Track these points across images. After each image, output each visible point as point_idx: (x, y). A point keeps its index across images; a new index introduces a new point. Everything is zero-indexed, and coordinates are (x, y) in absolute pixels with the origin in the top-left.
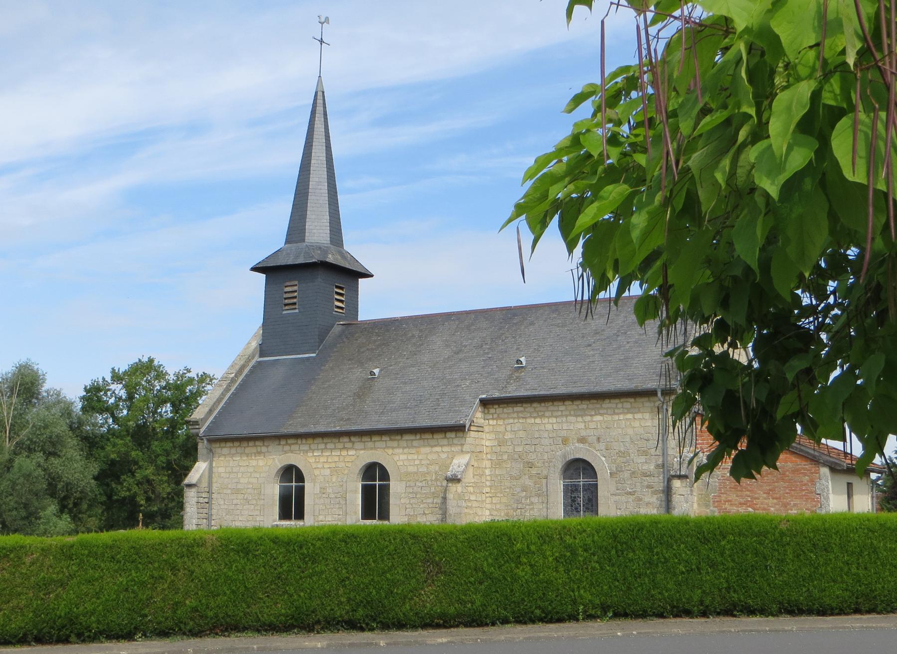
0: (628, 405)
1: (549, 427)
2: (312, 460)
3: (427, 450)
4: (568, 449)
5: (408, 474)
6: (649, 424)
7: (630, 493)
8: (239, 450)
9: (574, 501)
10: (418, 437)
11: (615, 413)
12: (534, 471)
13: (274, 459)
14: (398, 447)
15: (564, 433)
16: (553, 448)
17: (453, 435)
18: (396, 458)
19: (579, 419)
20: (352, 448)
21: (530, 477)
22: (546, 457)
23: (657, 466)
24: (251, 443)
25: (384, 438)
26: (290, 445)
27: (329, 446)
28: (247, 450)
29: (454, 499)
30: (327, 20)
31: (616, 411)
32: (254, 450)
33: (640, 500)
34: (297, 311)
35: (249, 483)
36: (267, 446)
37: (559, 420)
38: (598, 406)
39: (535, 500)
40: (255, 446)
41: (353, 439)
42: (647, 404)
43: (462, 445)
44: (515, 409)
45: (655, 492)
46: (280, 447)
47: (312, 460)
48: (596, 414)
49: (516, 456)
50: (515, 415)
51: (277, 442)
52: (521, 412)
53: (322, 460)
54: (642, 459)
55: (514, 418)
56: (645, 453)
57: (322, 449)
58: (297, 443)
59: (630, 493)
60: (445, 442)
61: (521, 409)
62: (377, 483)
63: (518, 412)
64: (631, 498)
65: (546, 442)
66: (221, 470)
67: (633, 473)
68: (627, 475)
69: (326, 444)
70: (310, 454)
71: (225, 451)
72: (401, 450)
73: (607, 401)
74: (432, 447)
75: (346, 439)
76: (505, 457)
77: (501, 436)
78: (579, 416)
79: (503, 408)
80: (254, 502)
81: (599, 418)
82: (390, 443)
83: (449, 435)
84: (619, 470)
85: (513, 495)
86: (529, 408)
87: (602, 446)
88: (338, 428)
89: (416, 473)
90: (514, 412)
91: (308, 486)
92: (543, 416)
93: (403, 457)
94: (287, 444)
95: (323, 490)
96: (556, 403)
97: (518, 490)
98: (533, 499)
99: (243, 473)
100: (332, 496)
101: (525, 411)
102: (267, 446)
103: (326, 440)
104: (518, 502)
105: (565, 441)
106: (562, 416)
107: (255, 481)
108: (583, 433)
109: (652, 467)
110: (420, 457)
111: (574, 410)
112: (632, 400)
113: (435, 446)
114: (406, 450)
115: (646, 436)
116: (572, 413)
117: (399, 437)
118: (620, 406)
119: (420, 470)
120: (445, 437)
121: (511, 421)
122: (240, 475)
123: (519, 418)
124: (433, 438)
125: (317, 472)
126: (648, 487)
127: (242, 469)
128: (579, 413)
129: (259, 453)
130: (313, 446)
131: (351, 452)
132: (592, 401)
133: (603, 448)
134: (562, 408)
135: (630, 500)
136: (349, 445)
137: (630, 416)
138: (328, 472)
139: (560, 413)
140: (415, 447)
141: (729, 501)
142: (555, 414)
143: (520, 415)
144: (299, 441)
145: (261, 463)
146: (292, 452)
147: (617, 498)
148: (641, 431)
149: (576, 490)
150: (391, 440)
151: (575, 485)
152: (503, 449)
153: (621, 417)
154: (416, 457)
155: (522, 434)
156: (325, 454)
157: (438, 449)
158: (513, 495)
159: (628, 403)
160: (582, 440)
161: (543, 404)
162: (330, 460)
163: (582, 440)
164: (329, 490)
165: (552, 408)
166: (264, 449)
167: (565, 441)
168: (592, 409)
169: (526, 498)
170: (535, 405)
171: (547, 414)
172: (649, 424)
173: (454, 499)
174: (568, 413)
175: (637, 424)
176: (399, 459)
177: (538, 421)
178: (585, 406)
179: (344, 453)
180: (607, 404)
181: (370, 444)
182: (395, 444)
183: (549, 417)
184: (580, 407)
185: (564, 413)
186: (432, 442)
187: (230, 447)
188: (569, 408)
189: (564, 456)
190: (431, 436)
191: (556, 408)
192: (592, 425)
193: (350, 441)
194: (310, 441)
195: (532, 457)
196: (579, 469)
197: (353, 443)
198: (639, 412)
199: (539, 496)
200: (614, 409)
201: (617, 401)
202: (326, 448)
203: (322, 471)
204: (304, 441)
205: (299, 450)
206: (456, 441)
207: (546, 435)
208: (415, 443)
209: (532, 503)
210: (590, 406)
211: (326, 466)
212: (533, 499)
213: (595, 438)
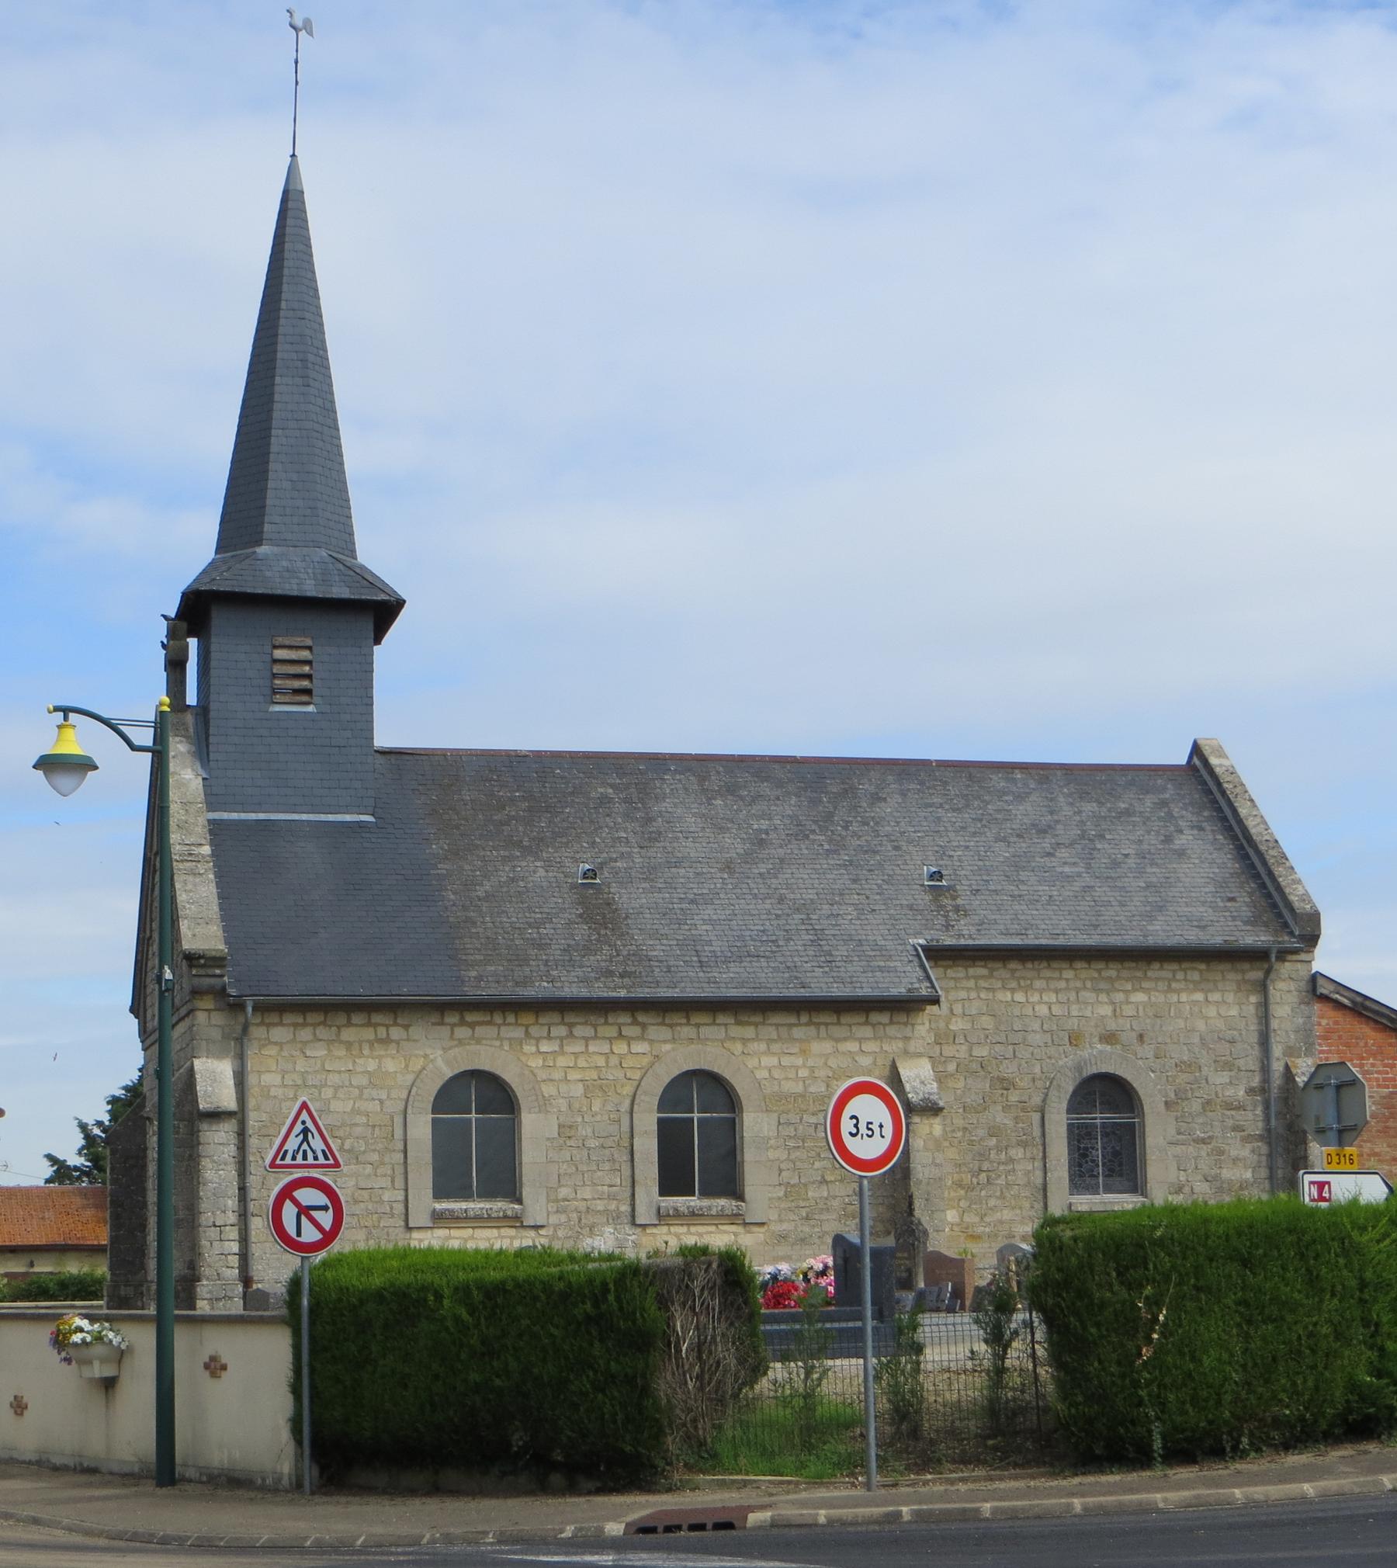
0: (1195, 976)
1: (1043, 1010)
2: (536, 1063)
3: (827, 1046)
4: (1085, 1054)
5: (781, 1097)
6: (1234, 1012)
7: (1203, 1141)
8: (322, 1032)
9: (1084, 1156)
10: (804, 1019)
11: (1170, 989)
12: (1014, 1097)
13: (433, 1056)
14: (757, 1039)
15: (1072, 1024)
16: (1052, 1051)
17: (884, 1018)
18: (752, 1062)
19: (1103, 997)
20: (642, 1038)
21: (1006, 1108)
22: (1037, 1070)
23: (1251, 1091)
24: (357, 1019)
25: (721, 1019)
26: (472, 1026)
27: (579, 1031)
28: (348, 1034)
29: (926, 1149)
30: (308, 26)
31: (1174, 985)
32: (368, 1034)
33: (1221, 1152)
34: (311, 708)
35: (355, 1111)
36: (406, 1027)
37: (1062, 997)
38: (1139, 974)
39: (1017, 1153)
40: (369, 1024)
41: (642, 1018)
42: (1231, 976)
43: (907, 1039)
44: (971, 971)
45: (1246, 1139)
46: (445, 1031)
47: (536, 1063)
48: (1134, 990)
49: (975, 1066)
50: (971, 983)
51: (435, 1017)
52: (983, 977)
53: (562, 1061)
54: (1223, 1078)
55: (969, 989)
56: (1228, 1066)
57: (561, 1039)
58: (490, 1023)
59: (1203, 1141)
60: (867, 1031)
61: (984, 971)
62: (696, 1115)
63: (976, 978)
64: (1204, 1150)
65: (1037, 1038)
66: (268, 1079)
67: (1209, 1102)
68: (1196, 1106)
69: (571, 1026)
70: (529, 1048)
71: (279, 1033)
72: (763, 1046)
73: (1156, 965)
74: (837, 1040)
75: (624, 1018)
76: (951, 1067)
77: (942, 1025)
78: (1101, 990)
79: (946, 967)
80: (375, 1157)
81: (1140, 997)
82: (736, 1031)
83: (875, 1017)
84: (1181, 1096)
85: (971, 1143)
86: (1026, 970)
87: (1147, 1051)
88: (623, 993)
89: (803, 1096)
90: (968, 978)
91: (529, 1122)
92: (1028, 988)
93: (769, 1061)
94: (463, 1023)
95: (566, 1130)
96: (1055, 965)
97: (981, 1132)
98: (1012, 1152)
99: (337, 1088)
100: (592, 1143)
101: (991, 976)
102: (406, 1027)
103: (570, 1018)
104: (982, 1156)
105: (1075, 1039)
106: (1067, 989)
107: (374, 1107)
108: (1112, 1025)
109: (1242, 1093)
110: (810, 1063)
111: (1092, 979)
112: (1203, 966)
113: (845, 1039)
114: (775, 1047)
115: (1229, 1034)
116: (1089, 984)
117: (758, 1018)
118: (1180, 975)
119: (812, 1089)
120: (867, 1023)
121: (963, 994)
122: (328, 1093)
123: (977, 988)
124: (839, 1023)
125: (548, 1090)
126: (1236, 1128)
127: (334, 1079)
128: (1102, 985)
129: (386, 1041)
130: (534, 1031)
131: (639, 1047)
132: (1127, 964)
133: (1151, 1055)
134: (1069, 974)
135: (1204, 1153)
136: (631, 1031)
137: (1199, 996)
138: (578, 1090)
139: (1062, 984)
140: (800, 1040)
141: (1376, 1154)
142: (1053, 984)
143: (982, 983)
144: (498, 1019)
145: (390, 1065)
146: (478, 1041)
147: (1178, 1150)
148: (1220, 1024)
149: (1089, 1134)
150: (738, 1023)
151: (1087, 1126)
152: (949, 1050)
153: (1184, 997)
154: (800, 1061)
155: (987, 1022)
156: (568, 1049)
157: (853, 1046)
158: (971, 1143)
159: (1195, 972)
160: (1109, 1038)
161: (1029, 965)
162: (582, 1063)
163: (1109, 1038)
164: (585, 1131)
165: (1047, 973)
166: (396, 1033)
167: (1075, 1039)
168: (1127, 980)
169: (999, 1150)
170: (1013, 965)
171: (1038, 984)
172: (1234, 1012)
173: (926, 1149)
174: (1079, 984)
175: (1212, 1012)
176: (767, 1068)
177: (1020, 997)
178: (1113, 973)
179: (621, 1048)
180: (1155, 971)
181: (687, 1031)
182: (749, 1032)
183: (1041, 991)
184: (1105, 974)
185: (1072, 984)
186: (836, 1031)
187: (295, 1025)
188: (1084, 974)
189: (1079, 1068)
190: (834, 1019)
191: (1056, 974)
192: (1129, 1010)
193: (635, 1022)
194: (528, 1018)
195: (1009, 1069)
196: (1107, 1096)
197: (644, 1026)
198: (1216, 989)
199: (1024, 1144)
200: (1169, 980)
201: (1175, 966)
202: (571, 1035)
203: (563, 1088)
204: (511, 1018)
205: (499, 1038)
206: (892, 1030)
207: (1036, 1026)
208: (798, 1032)
209: (1012, 1160)
210: (1125, 973)
211: (574, 1075)
212: (1012, 1152)
213: (1134, 1035)
